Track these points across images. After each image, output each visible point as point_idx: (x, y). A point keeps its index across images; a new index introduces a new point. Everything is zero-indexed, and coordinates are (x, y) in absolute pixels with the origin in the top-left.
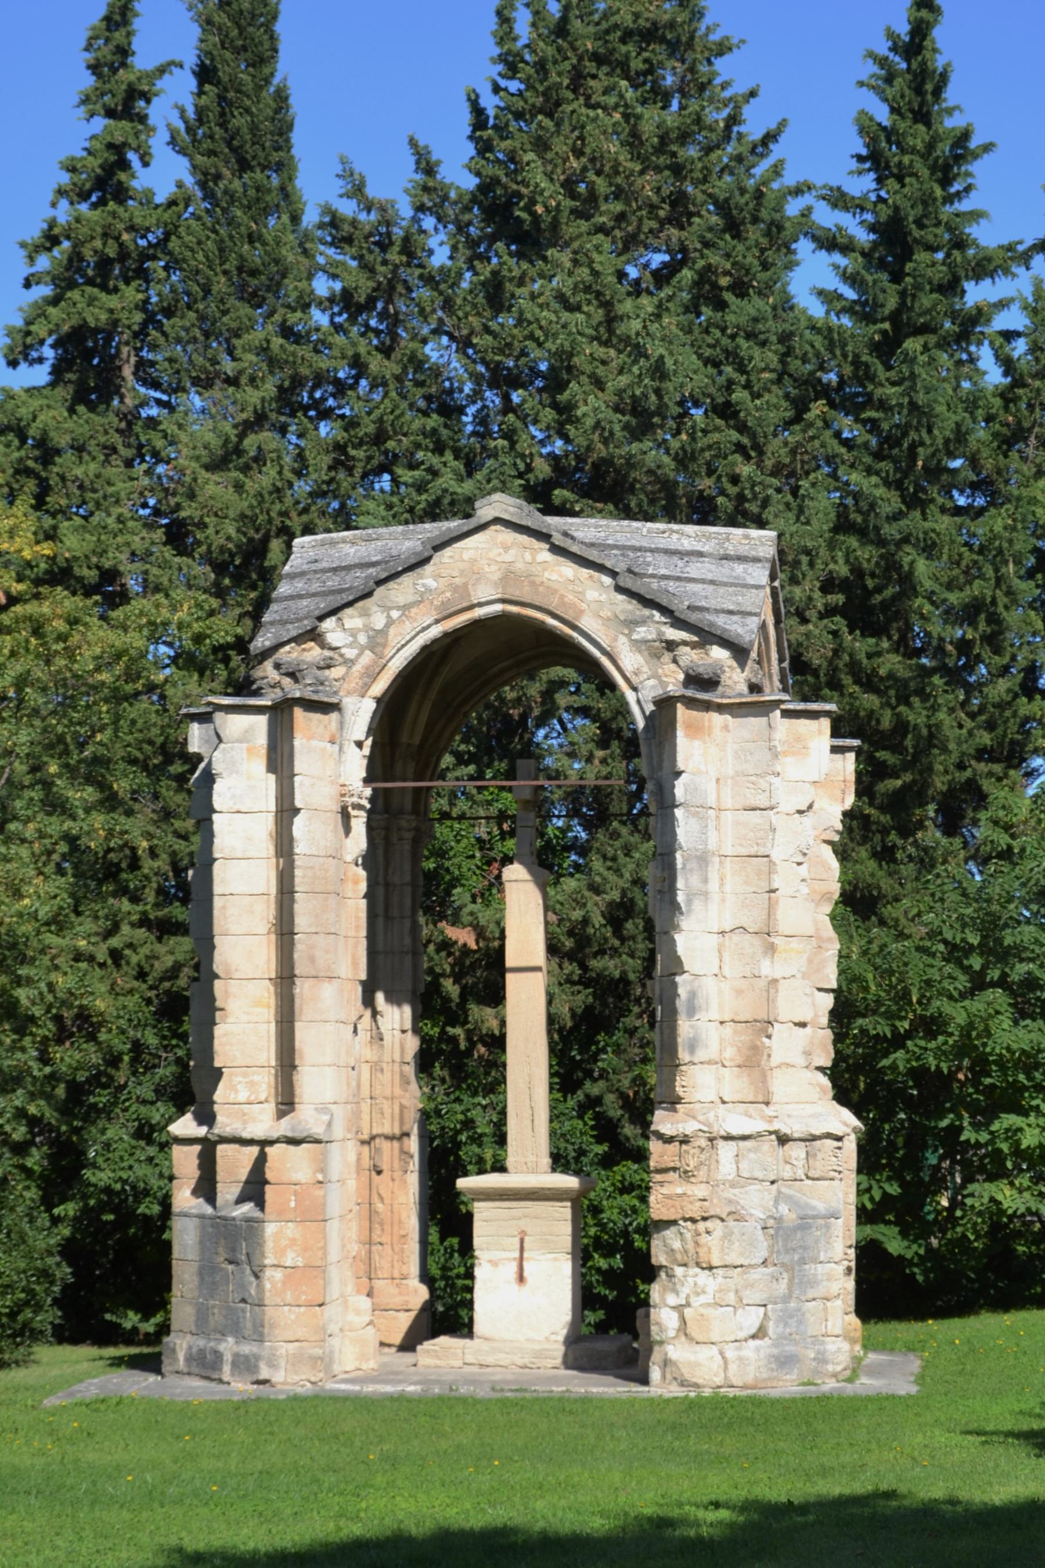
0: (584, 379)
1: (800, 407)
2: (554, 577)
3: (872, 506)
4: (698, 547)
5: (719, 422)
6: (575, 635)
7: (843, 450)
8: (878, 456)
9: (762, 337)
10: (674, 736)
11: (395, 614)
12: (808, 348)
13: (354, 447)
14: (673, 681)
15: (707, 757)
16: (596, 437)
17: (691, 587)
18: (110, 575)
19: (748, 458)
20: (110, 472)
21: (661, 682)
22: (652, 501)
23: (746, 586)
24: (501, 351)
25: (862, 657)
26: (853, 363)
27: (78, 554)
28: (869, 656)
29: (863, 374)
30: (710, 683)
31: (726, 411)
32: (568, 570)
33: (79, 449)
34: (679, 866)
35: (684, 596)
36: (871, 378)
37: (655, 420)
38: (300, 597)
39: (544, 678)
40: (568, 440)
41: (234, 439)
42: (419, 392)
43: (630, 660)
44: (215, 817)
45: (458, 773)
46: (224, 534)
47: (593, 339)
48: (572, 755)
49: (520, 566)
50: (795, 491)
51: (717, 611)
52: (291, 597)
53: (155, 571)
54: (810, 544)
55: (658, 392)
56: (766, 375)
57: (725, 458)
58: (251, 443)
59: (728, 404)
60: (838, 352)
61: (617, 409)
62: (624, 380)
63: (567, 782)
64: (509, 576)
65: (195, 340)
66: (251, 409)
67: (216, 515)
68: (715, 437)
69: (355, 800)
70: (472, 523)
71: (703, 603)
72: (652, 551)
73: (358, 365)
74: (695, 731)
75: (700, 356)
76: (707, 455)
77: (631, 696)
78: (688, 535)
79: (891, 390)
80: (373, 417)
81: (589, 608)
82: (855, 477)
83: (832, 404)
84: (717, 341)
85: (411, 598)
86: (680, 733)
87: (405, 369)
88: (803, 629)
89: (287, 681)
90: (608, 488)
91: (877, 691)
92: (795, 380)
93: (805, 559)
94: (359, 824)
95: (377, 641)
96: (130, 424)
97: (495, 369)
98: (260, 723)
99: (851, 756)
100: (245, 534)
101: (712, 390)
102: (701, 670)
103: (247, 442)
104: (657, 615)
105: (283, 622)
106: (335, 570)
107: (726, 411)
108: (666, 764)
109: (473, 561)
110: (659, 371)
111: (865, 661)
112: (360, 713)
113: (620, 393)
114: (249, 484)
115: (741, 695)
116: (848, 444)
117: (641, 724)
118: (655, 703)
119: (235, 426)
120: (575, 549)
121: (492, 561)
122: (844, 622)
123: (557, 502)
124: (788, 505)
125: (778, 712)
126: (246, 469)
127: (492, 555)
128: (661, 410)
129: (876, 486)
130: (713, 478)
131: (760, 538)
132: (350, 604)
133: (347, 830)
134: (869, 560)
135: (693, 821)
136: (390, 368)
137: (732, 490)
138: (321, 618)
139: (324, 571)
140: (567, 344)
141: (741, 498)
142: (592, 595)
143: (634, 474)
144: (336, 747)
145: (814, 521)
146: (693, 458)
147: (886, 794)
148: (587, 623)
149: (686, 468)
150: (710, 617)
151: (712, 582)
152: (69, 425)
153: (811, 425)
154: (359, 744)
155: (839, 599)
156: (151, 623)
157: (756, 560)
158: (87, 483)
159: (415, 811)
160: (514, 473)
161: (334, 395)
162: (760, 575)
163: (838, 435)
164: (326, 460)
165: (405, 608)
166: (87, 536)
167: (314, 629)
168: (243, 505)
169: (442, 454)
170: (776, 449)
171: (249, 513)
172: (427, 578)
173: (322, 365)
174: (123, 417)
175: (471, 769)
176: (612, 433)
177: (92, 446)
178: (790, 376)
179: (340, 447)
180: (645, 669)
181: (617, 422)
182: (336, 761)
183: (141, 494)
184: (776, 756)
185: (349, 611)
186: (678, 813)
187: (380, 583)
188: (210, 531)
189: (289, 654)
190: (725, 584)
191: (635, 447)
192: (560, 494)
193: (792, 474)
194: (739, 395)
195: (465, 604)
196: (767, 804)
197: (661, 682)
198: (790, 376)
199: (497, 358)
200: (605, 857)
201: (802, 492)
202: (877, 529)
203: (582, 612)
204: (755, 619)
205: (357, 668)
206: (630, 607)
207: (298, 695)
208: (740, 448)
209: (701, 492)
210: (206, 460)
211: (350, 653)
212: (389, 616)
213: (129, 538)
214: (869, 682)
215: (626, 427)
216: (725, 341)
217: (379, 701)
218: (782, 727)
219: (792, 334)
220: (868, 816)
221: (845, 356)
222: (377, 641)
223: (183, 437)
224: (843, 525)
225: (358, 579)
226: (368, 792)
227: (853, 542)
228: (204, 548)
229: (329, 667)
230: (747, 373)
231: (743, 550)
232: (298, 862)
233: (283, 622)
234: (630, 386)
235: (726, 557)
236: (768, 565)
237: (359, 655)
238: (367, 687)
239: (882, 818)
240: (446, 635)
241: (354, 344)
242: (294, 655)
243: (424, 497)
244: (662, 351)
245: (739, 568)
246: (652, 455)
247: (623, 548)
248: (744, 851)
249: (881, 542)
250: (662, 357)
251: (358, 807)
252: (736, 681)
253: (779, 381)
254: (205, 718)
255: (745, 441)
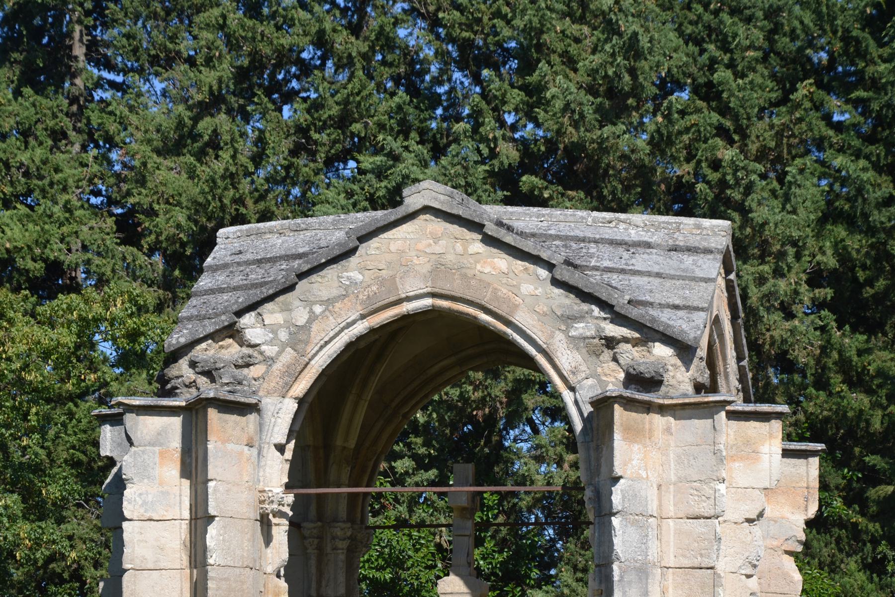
0: (555, 58)
1: (787, 86)
2: (487, 270)
3: (860, 191)
4: (646, 238)
5: (700, 103)
6: (509, 331)
7: (831, 133)
8: (870, 139)
9: (747, 12)
10: (612, 440)
11: (318, 309)
12: (796, 23)
13: (319, 131)
14: (612, 380)
15: (646, 462)
16: (566, 120)
17: (636, 280)
18: (55, 268)
19: (731, 142)
20: (59, 158)
21: (600, 381)
22: (627, 189)
23: (694, 279)
24: (469, 27)
25: (852, 354)
26: (842, 39)
27: (19, 244)
28: (860, 353)
29: (853, 48)
30: (652, 383)
31: (708, 92)
32: (502, 262)
33: (26, 134)
34: (616, 578)
35: (623, 290)
36: (863, 54)
37: (630, 101)
38: (221, 290)
39: (510, 376)
40: (538, 125)
41: (189, 123)
42: (386, 72)
43: (568, 358)
44: (125, 525)
45: (417, 479)
46: (172, 222)
47: (564, 15)
48: (540, 459)
49: (450, 258)
50: (781, 179)
51: (661, 306)
52: (212, 291)
53: (97, 261)
54: (795, 234)
55: (632, 72)
56: (751, 54)
57: (705, 142)
58: (205, 125)
59: (710, 84)
60: (827, 27)
61: (591, 90)
62: (597, 59)
63: (534, 488)
64: (439, 268)
65: (155, 16)
66: (206, 89)
67: (167, 202)
68: (694, 118)
69: (275, 506)
70: (400, 211)
71: (648, 298)
72: (596, 241)
73: (321, 41)
74: (634, 434)
75: (680, 31)
76: (686, 138)
77: (568, 397)
78: (637, 224)
79: (882, 67)
80: (338, 98)
81: (524, 302)
82: (839, 161)
83: (819, 85)
84: (699, 17)
85: (335, 292)
86: (617, 436)
87: (372, 48)
88: (788, 325)
89: (202, 381)
90: (581, 176)
91: (869, 392)
92: (782, 59)
93: (791, 251)
94: (281, 532)
95: (298, 337)
96: (81, 108)
97: (465, 46)
98: (175, 423)
99: (815, 461)
100: (196, 222)
101: (693, 69)
102: (642, 369)
103: (201, 125)
104: (596, 310)
105: (201, 318)
106: (259, 262)
107: (708, 92)
108: (604, 469)
109: (401, 252)
110: (633, 50)
111: (855, 358)
112: (281, 414)
113: (593, 73)
114: (200, 169)
115: (685, 395)
116: (839, 127)
117: (578, 426)
118: (592, 404)
119: (189, 108)
120: (509, 239)
121: (421, 253)
122: (832, 317)
123: (525, 189)
124: (773, 192)
125: (723, 414)
126: (200, 155)
127: (421, 246)
128: (636, 90)
129: (864, 170)
130: (693, 164)
131: (712, 228)
132: (270, 298)
133: (268, 539)
134: (858, 251)
135: (631, 530)
136: (358, 46)
137: (713, 176)
138: (240, 313)
139: (248, 263)
140: (535, 20)
141: (723, 184)
142: (527, 288)
143: (610, 159)
144: (254, 451)
145: (801, 210)
146: (670, 143)
147: (878, 502)
148: (521, 318)
149: (663, 153)
150: (652, 312)
151: (658, 275)
152: (14, 107)
153: (798, 106)
154: (281, 448)
155: (827, 293)
156: (81, 318)
157: (708, 251)
158: (33, 169)
159: (351, 519)
160: (476, 158)
161: (298, 78)
162: (712, 267)
163: (827, 118)
164: (286, 145)
165: (329, 303)
166: (30, 226)
167: (232, 325)
168: (194, 190)
169: (406, 138)
170: (761, 131)
171: (201, 199)
172: (351, 271)
173: (283, 41)
174: (74, 100)
175: (432, 474)
176: (582, 116)
177: (39, 130)
178: (778, 54)
179: (302, 130)
180: (583, 368)
181: (588, 105)
182: (255, 466)
183: (91, 181)
184: (721, 460)
185: (269, 306)
186: (615, 521)
187: (302, 276)
188: (161, 219)
189: (205, 352)
190: (672, 277)
191: (608, 130)
192: (528, 180)
193: (779, 159)
194: (722, 74)
195: (392, 299)
196: (711, 512)
197: (600, 381)
198: (778, 54)
199: (465, 34)
200: (575, 568)
201: (789, 178)
202: (865, 216)
203: (516, 306)
204: (703, 314)
205: (278, 366)
206: (567, 302)
207: (212, 395)
208: (721, 132)
209: (680, 178)
210: (158, 144)
211: (270, 350)
212: (311, 311)
213: (75, 227)
214: (857, 380)
215: (599, 109)
216: (707, 17)
217: (301, 401)
218: (730, 431)
219: (780, 9)
220: (855, 525)
221: (835, 32)
222: (298, 337)
223: (134, 119)
224: (830, 215)
225: (278, 274)
226: (290, 498)
227: (841, 231)
228: (153, 237)
229: (248, 365)
230: (731, 51)
231: (694, 241)
232: (211, 574)
233: (201, 318)
234: (603, 65)
235: (675, 249)
236: (720, 257)
237: (280, 353)
238: (289, 386)
239: (871, 526)
240: (372, 331)
241: (320, 20)
242: (211, 352)
243: (383, 184)
244: (635, 27)
245: (688, 260)
246: (631, 140)
247: (566, 238)
248: (687, 563)
249: (871, 231)
250: (635, 34)
251: (280, 514)
252: (680, 380)
253: (765, 59)
254: (116, 420)
255: (728, 124)
